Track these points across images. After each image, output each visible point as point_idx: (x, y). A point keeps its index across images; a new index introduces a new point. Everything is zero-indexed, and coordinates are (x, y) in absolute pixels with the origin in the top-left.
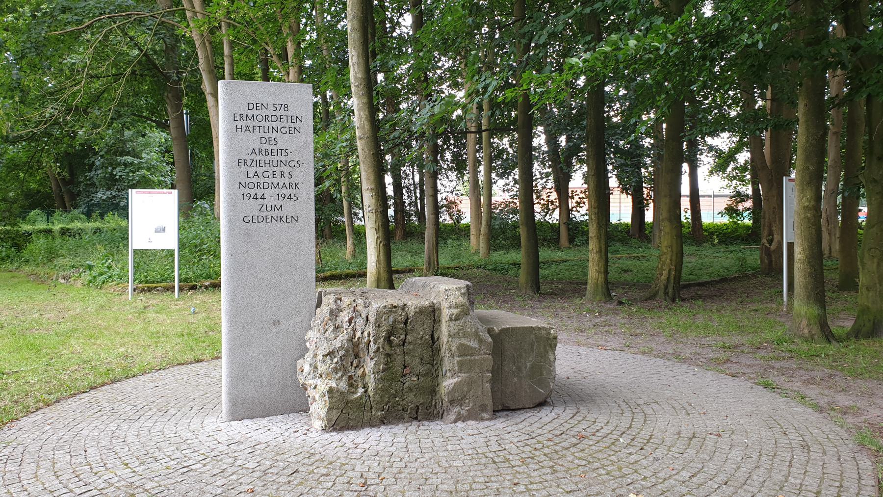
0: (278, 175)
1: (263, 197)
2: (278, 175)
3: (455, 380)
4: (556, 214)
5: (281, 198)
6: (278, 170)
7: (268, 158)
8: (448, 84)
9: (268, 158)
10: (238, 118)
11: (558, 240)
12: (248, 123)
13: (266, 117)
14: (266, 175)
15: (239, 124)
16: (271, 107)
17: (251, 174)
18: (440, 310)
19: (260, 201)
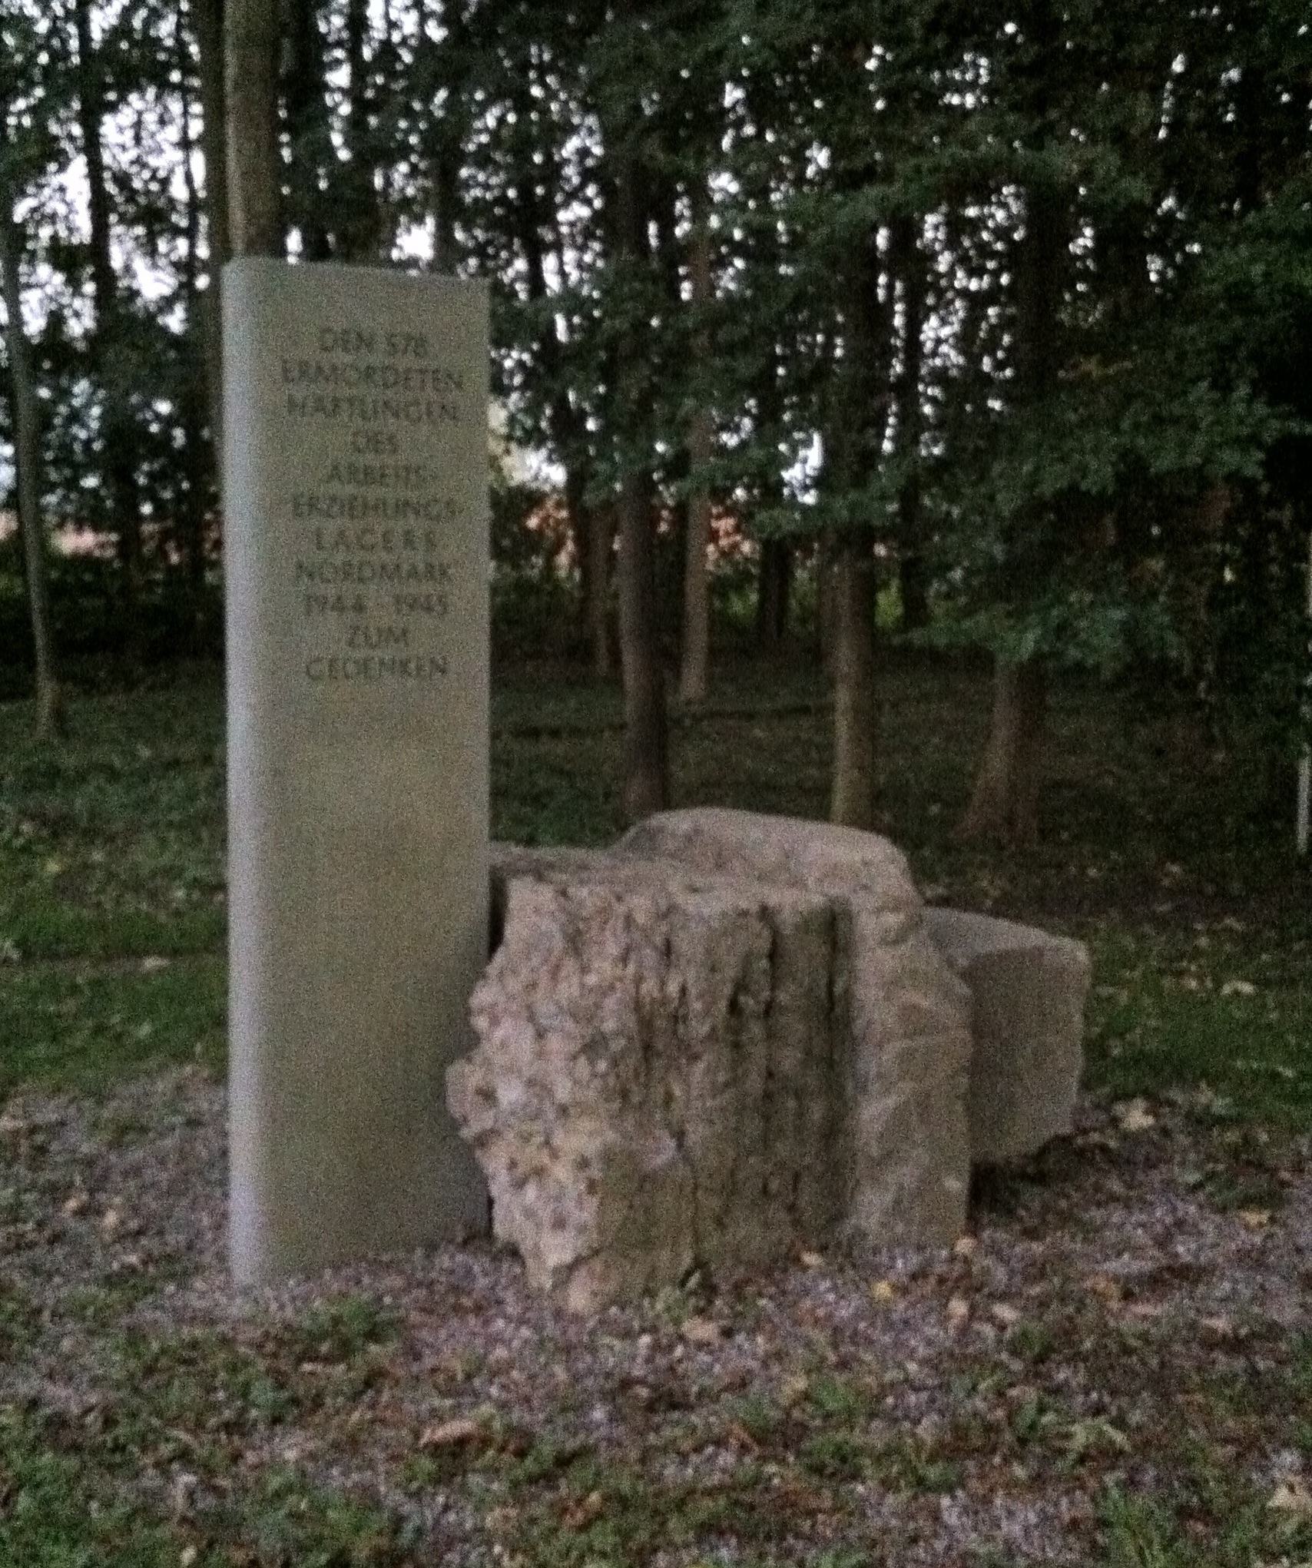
0: (397, 540)
1: (359, 608)
2: (397, 540)
3: (891, 1101)
4: (892, 507)
5: (405, 608)
6: (399, 526)
7: (374, 493)
8: (1133, 690)
9: (374, 493)
10: (296, 374)
11: (824, 790)
12: (317, 389)
13: (369, 373)
14: (368, 539)
15: (299, 393)
16: (382, 345)
17: (328, 540)
18: (850, 917)
19: (350, 616)
